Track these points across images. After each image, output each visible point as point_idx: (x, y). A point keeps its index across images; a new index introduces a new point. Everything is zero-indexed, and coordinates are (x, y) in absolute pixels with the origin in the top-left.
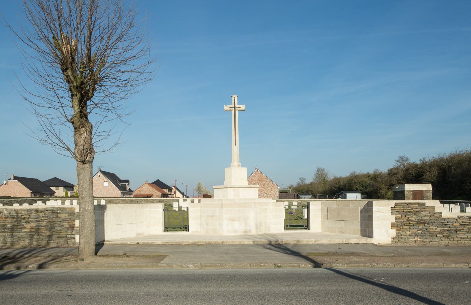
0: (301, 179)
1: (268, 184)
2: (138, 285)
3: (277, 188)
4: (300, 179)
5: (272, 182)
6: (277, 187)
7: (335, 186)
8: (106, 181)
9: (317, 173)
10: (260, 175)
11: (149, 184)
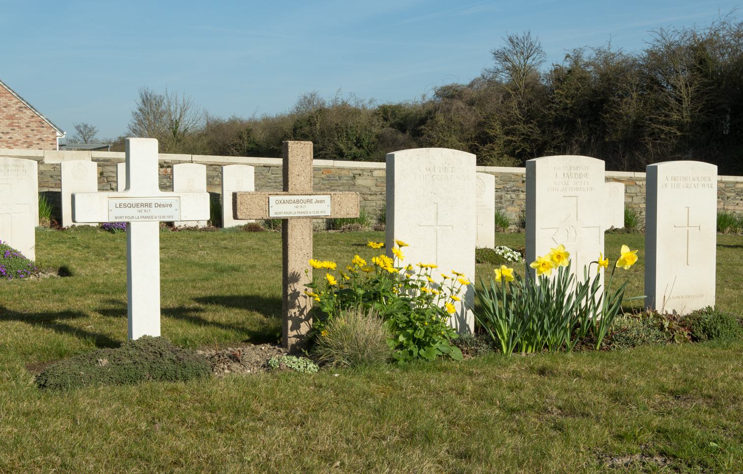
0: (82, 129)
3: (52, 137)
4: (78, 128)
6: (54, 133)
9: (141, 110)
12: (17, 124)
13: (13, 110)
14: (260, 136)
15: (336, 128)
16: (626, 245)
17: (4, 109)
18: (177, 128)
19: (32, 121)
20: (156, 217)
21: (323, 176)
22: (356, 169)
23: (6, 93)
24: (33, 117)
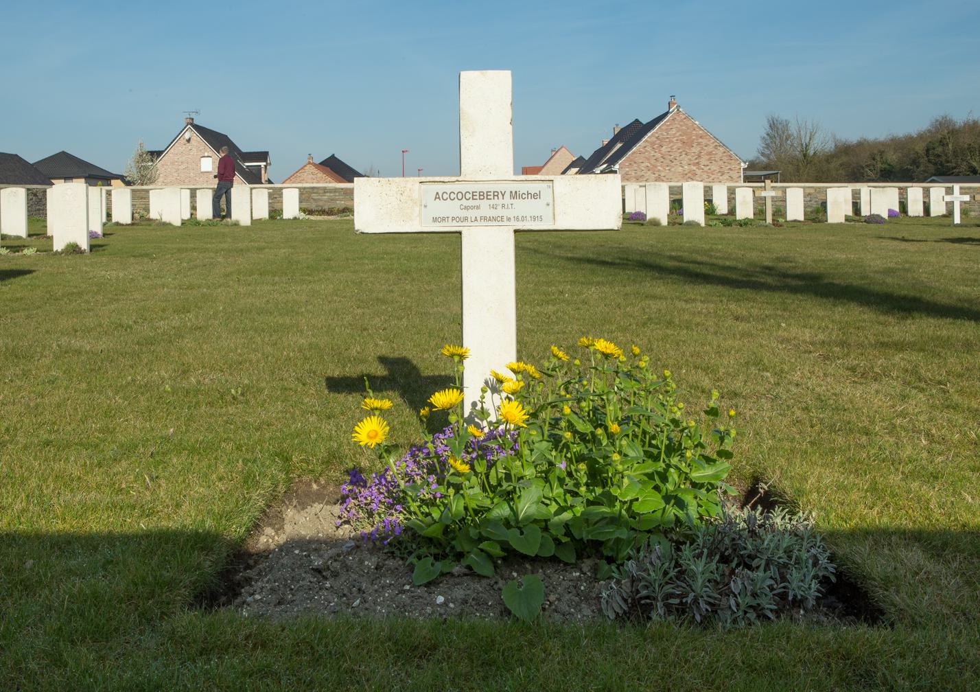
1: (710, 153)
6: (740, 164)
8: (206, 155)
9: (768, 135)
11: (315, 165)
14: (893, 157)
15: (969, 148)
16: (188, 220)
18: (807, 151)
20: (509, 219)
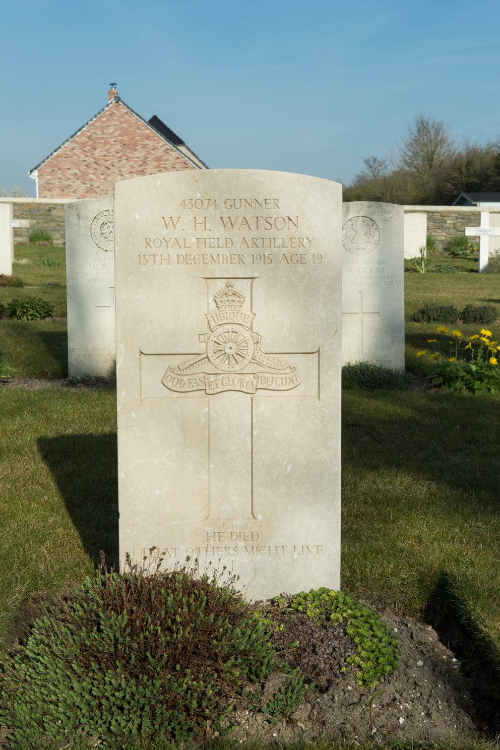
0: (371, 163)
1: (158, 159)
2: (455, 371)
4: (367, 162)
5: (173, 154)
7: (453, 179)
10: (127, 121)
12: (163, 166)
13: (161, 153)
17: (152, 152)
19: (177, 163)
21: (26, 209)
22: (51, 204)
23: (154, 136)
24: (178, 158)
